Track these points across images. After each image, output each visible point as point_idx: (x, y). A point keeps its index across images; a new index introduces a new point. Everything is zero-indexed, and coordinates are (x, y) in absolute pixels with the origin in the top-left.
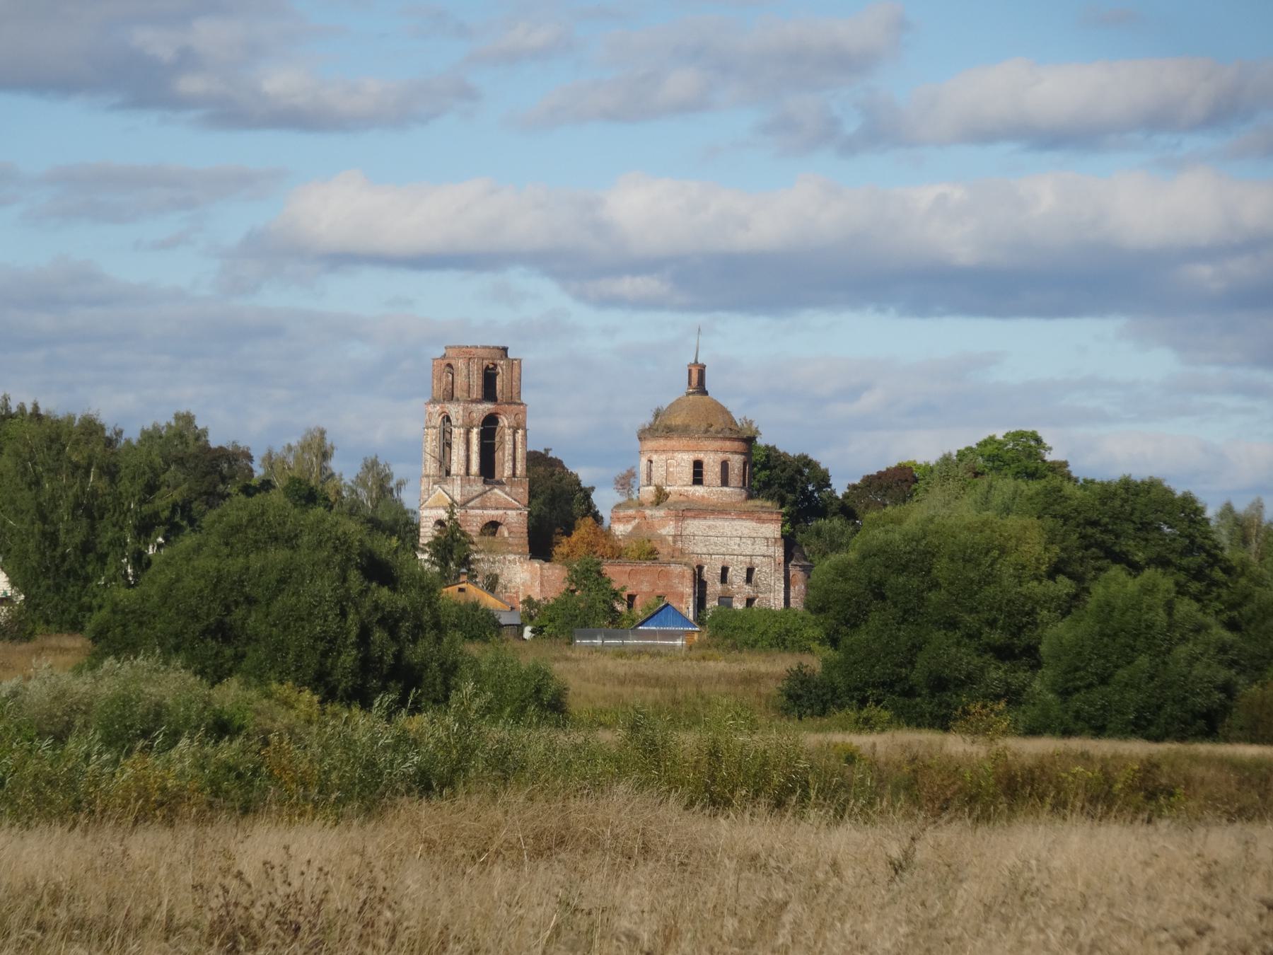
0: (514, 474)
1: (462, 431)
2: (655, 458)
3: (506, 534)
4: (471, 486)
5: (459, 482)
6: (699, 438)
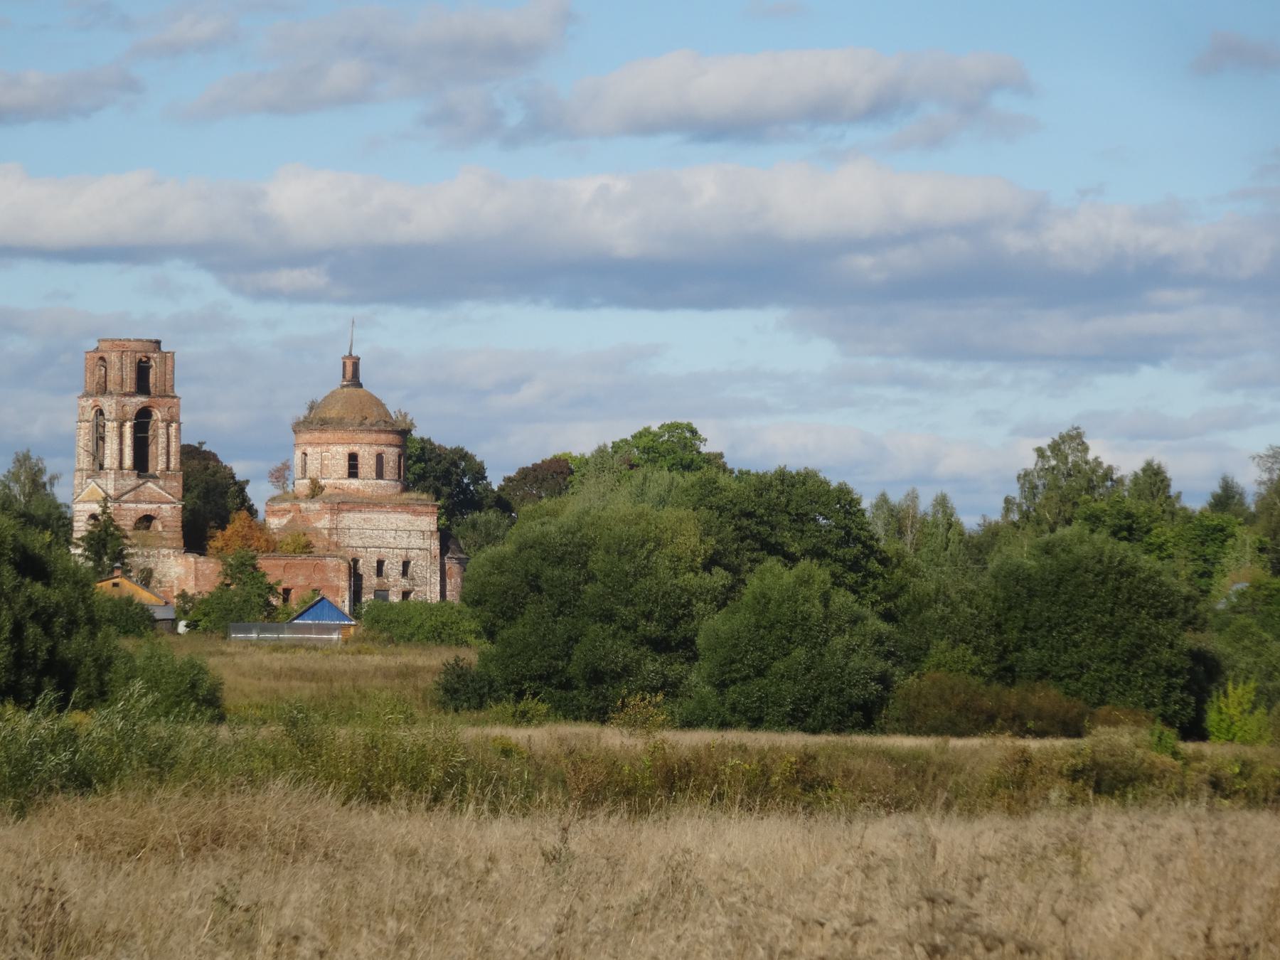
0: (168, 468)
1: (115, 424)
2: (309, 450)
4: (125, 480)
5: (113, 476)
6: (354, 431)
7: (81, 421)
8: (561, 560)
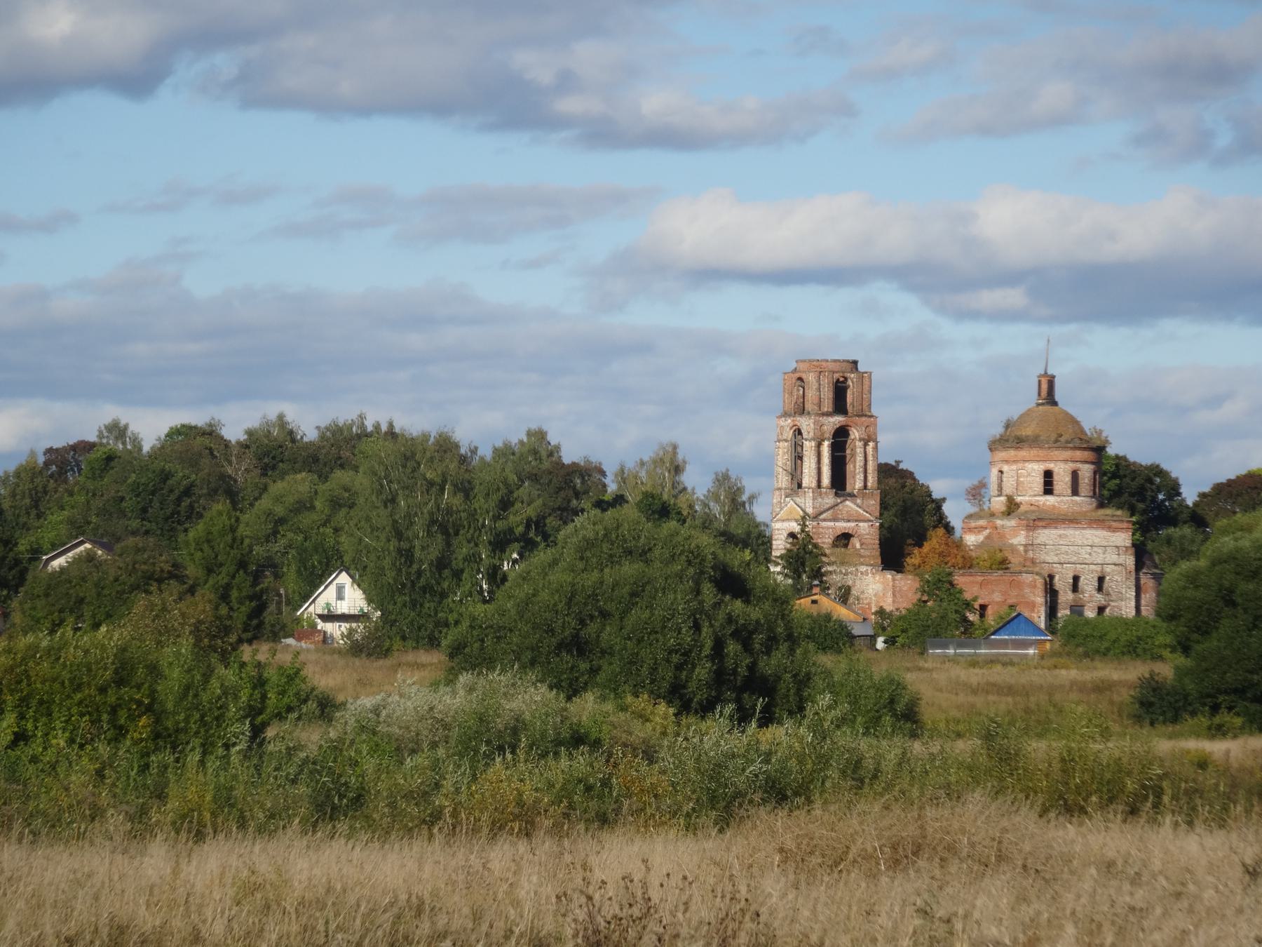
0: (865, 487)
1: (813, 444)
2: (1005, 468)
3: (858, 546)
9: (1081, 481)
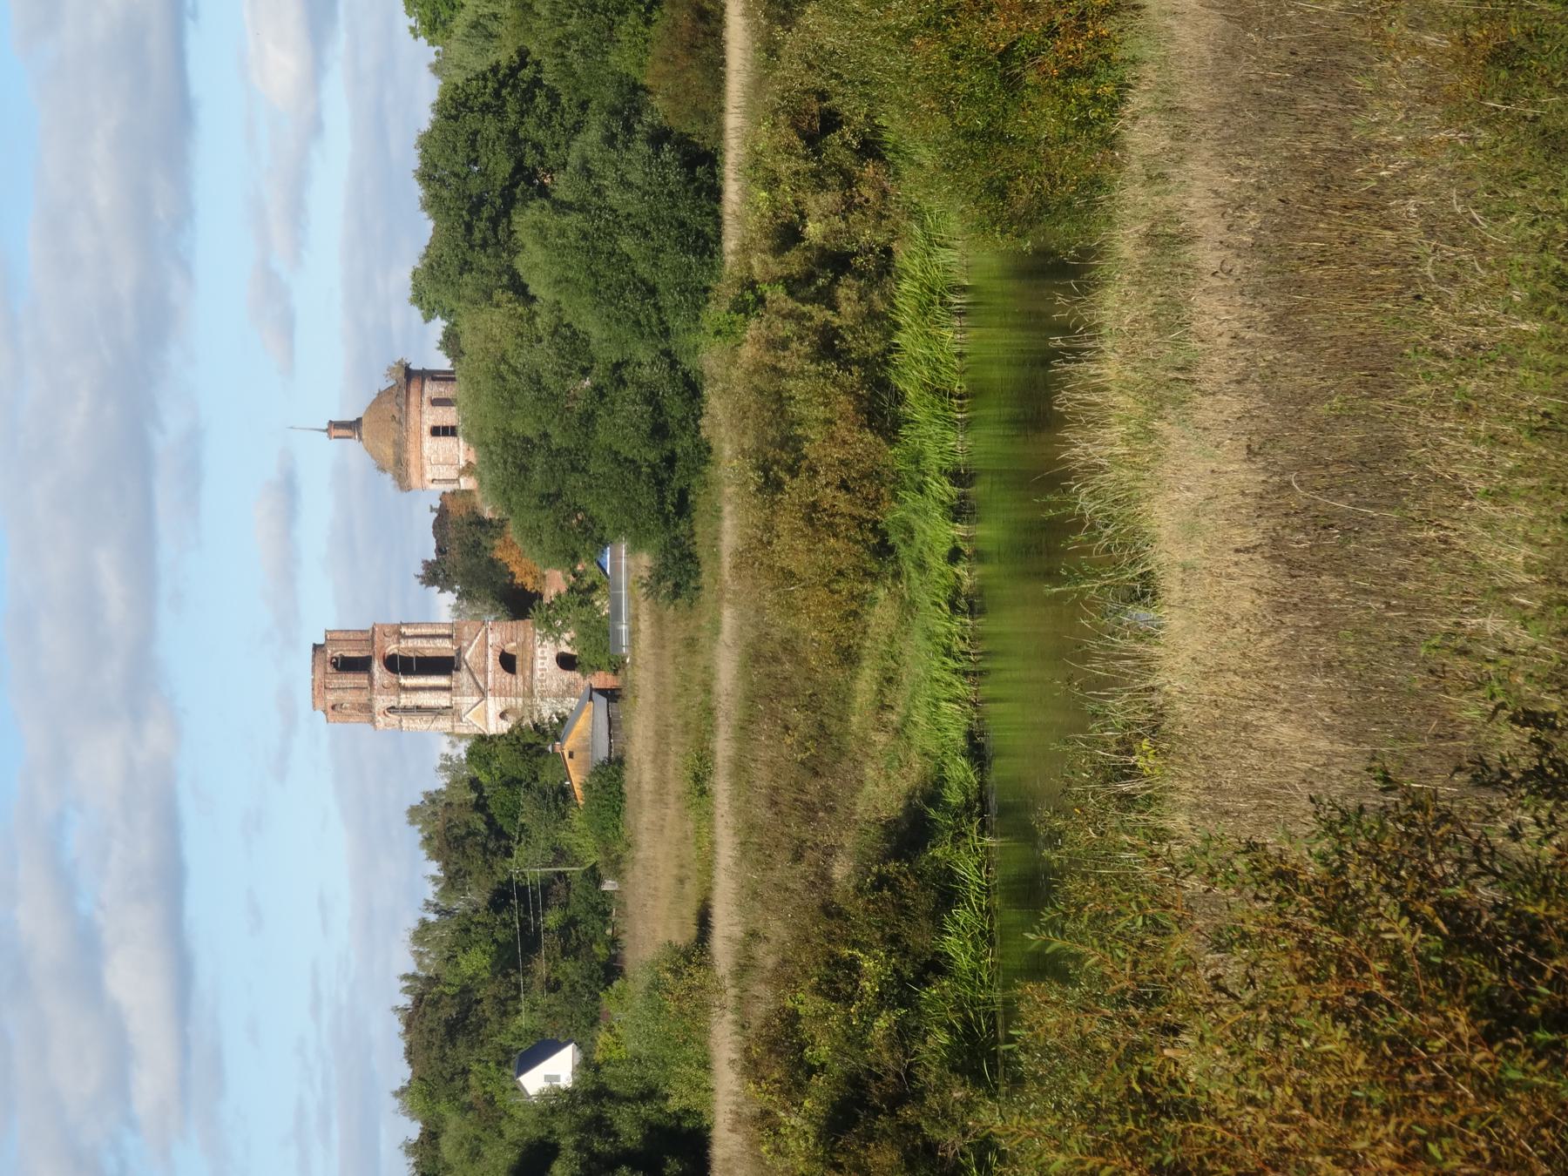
0: (450, 636)
1: (403, 696)
2: (429, 476)
3: (514, 644)
7: (401, 727)
8: (524, 469)
9: (443, 396)
